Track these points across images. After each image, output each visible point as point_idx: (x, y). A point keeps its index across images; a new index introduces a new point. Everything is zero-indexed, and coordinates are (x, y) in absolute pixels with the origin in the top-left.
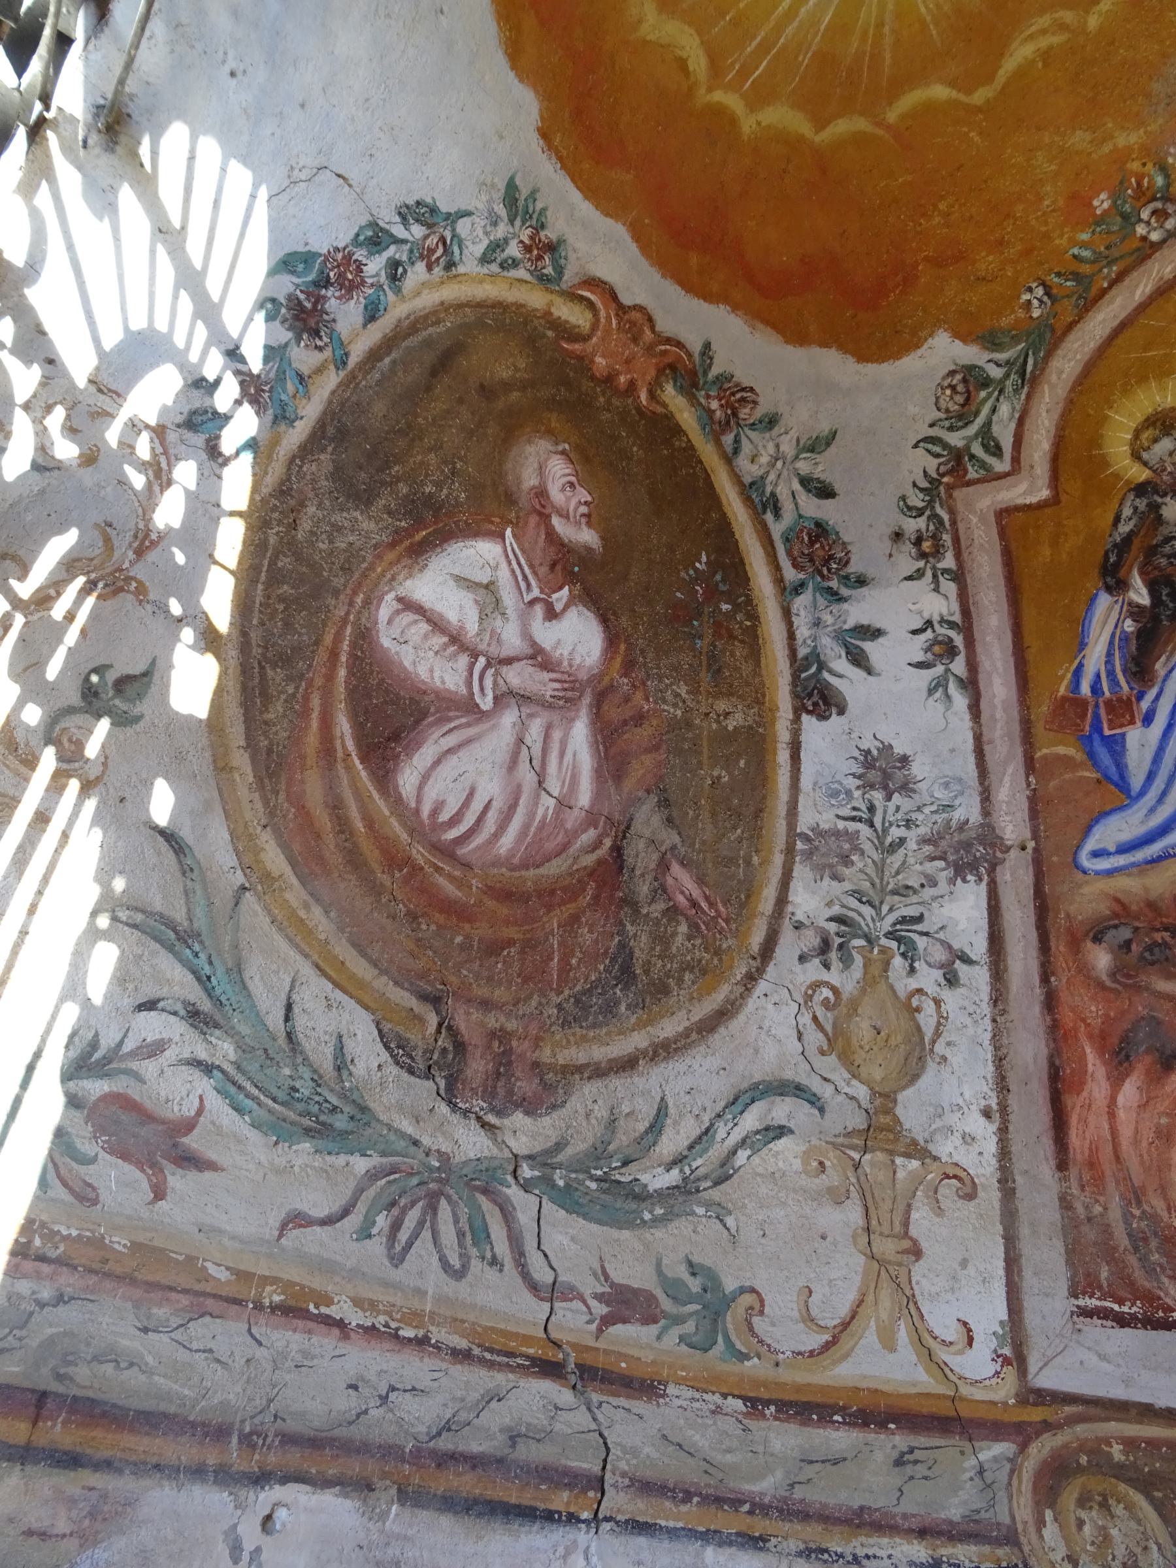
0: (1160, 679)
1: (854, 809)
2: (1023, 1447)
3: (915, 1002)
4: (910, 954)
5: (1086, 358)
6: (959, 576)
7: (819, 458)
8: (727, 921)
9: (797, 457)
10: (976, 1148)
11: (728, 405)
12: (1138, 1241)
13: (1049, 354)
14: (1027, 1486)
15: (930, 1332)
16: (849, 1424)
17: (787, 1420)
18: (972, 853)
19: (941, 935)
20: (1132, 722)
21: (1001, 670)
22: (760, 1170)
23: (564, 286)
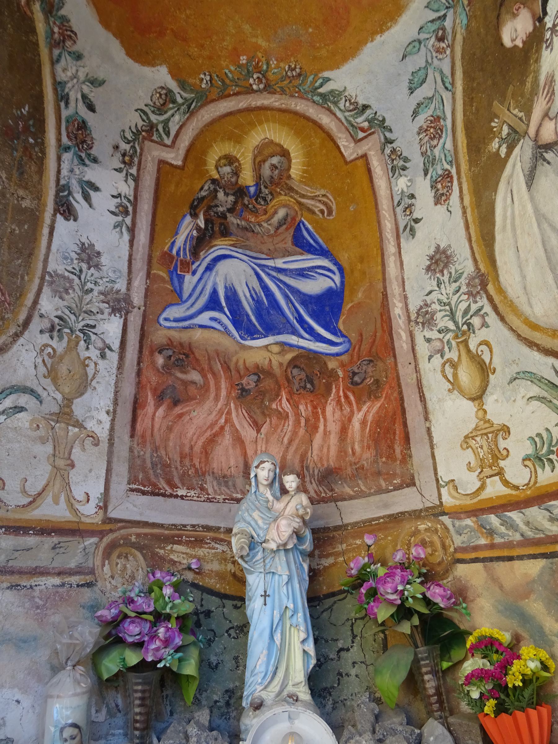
1: (74, 268)
2: (101, 539)
3: (87, 362)
4: (88, 341)
5: (214, 117)
6: (136, 180)
7: (94, 89)
8: (9, 304)
9: (84, 82)
10: (102, 426)
12: (154, 465)
13: (201, 107)
14: (100, 553)
15: (73, 497)
16: (36, 534)
17: (9, 534)
18: (119, 305)
19: (102, 336)
20: (188, 272)
22: (10, 426)
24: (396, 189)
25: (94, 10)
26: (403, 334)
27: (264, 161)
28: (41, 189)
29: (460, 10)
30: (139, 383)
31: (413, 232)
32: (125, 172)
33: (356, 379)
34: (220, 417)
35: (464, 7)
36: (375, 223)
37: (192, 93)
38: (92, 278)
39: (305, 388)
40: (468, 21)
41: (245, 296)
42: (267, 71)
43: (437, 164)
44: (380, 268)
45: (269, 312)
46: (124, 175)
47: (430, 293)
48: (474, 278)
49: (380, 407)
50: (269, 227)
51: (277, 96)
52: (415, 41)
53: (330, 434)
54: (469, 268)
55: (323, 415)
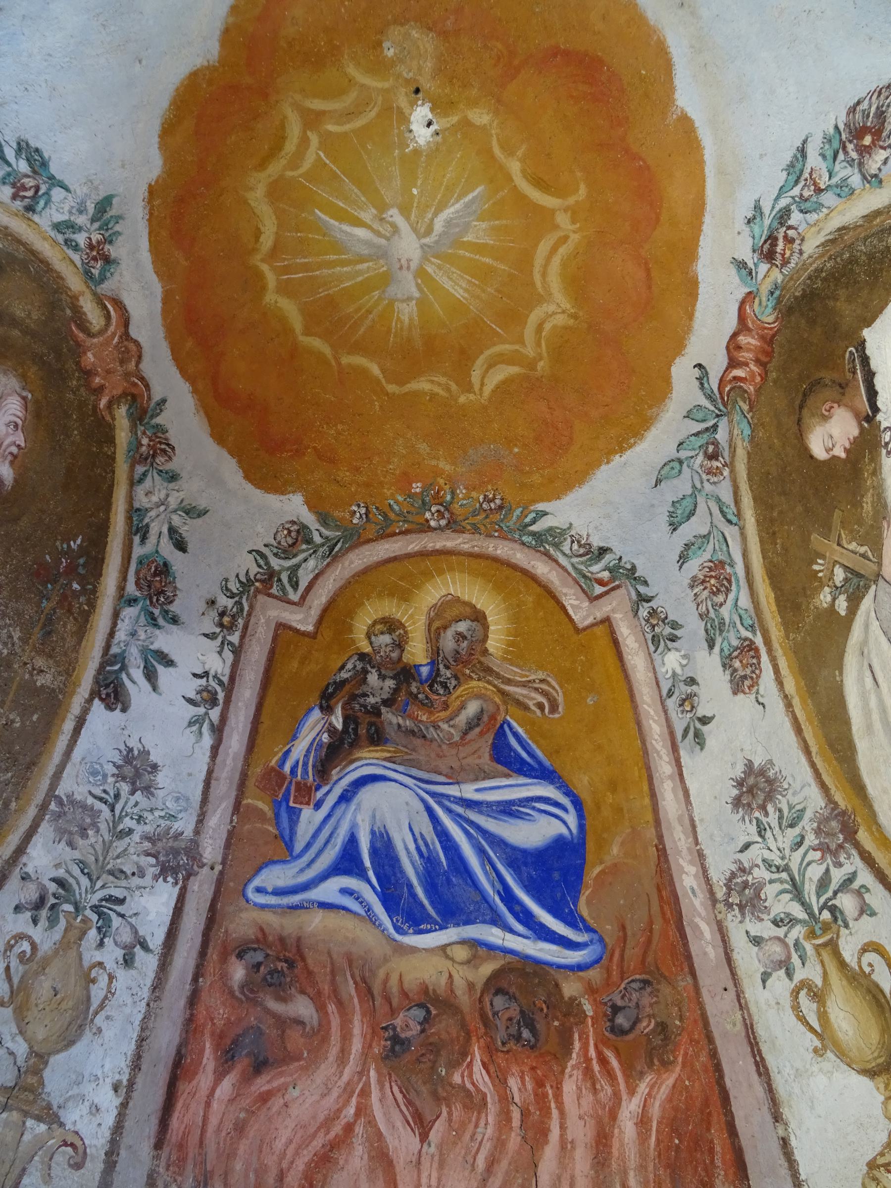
0: (332, 782)
1: (105, 791)
3: (93, 974)
4: (103, 931)
5: (369, 563)
6: (237, 652)
7: (189, 521)
9: (175, 511)
11: (153, 447)
19: (133, 920)
20: (308, 803)
21: (240, 730)
23: (99, 290)
24: (664, 670)
25: (206, 420)
26: (704, 927)
27: (445, 628)
28: (77, 659)
29: (737, 417)
30: (190, 1020)
31: (700, 740)
32: (220, 639)
33: (620, 1020)
34: (348, 1101)
35: (743, 413)
36: (633, 725)
37: (338, 530)
38: (135, 810)
39: (518, 1038)
40: (753, 431)
41: (407, 849)
42: (451, 503)
43: (728, 631)
44: (647, 801)
45: (448, 881)
46: (219, 644)
47: (747, 846)
48: (827, 820)
49: (674, 1086)
50: (452, 730)
51: (467, 536)
52: (673, 460)
53: (573, 1148)
54: (815, 801)
55: (556, 1102)
